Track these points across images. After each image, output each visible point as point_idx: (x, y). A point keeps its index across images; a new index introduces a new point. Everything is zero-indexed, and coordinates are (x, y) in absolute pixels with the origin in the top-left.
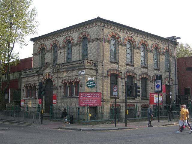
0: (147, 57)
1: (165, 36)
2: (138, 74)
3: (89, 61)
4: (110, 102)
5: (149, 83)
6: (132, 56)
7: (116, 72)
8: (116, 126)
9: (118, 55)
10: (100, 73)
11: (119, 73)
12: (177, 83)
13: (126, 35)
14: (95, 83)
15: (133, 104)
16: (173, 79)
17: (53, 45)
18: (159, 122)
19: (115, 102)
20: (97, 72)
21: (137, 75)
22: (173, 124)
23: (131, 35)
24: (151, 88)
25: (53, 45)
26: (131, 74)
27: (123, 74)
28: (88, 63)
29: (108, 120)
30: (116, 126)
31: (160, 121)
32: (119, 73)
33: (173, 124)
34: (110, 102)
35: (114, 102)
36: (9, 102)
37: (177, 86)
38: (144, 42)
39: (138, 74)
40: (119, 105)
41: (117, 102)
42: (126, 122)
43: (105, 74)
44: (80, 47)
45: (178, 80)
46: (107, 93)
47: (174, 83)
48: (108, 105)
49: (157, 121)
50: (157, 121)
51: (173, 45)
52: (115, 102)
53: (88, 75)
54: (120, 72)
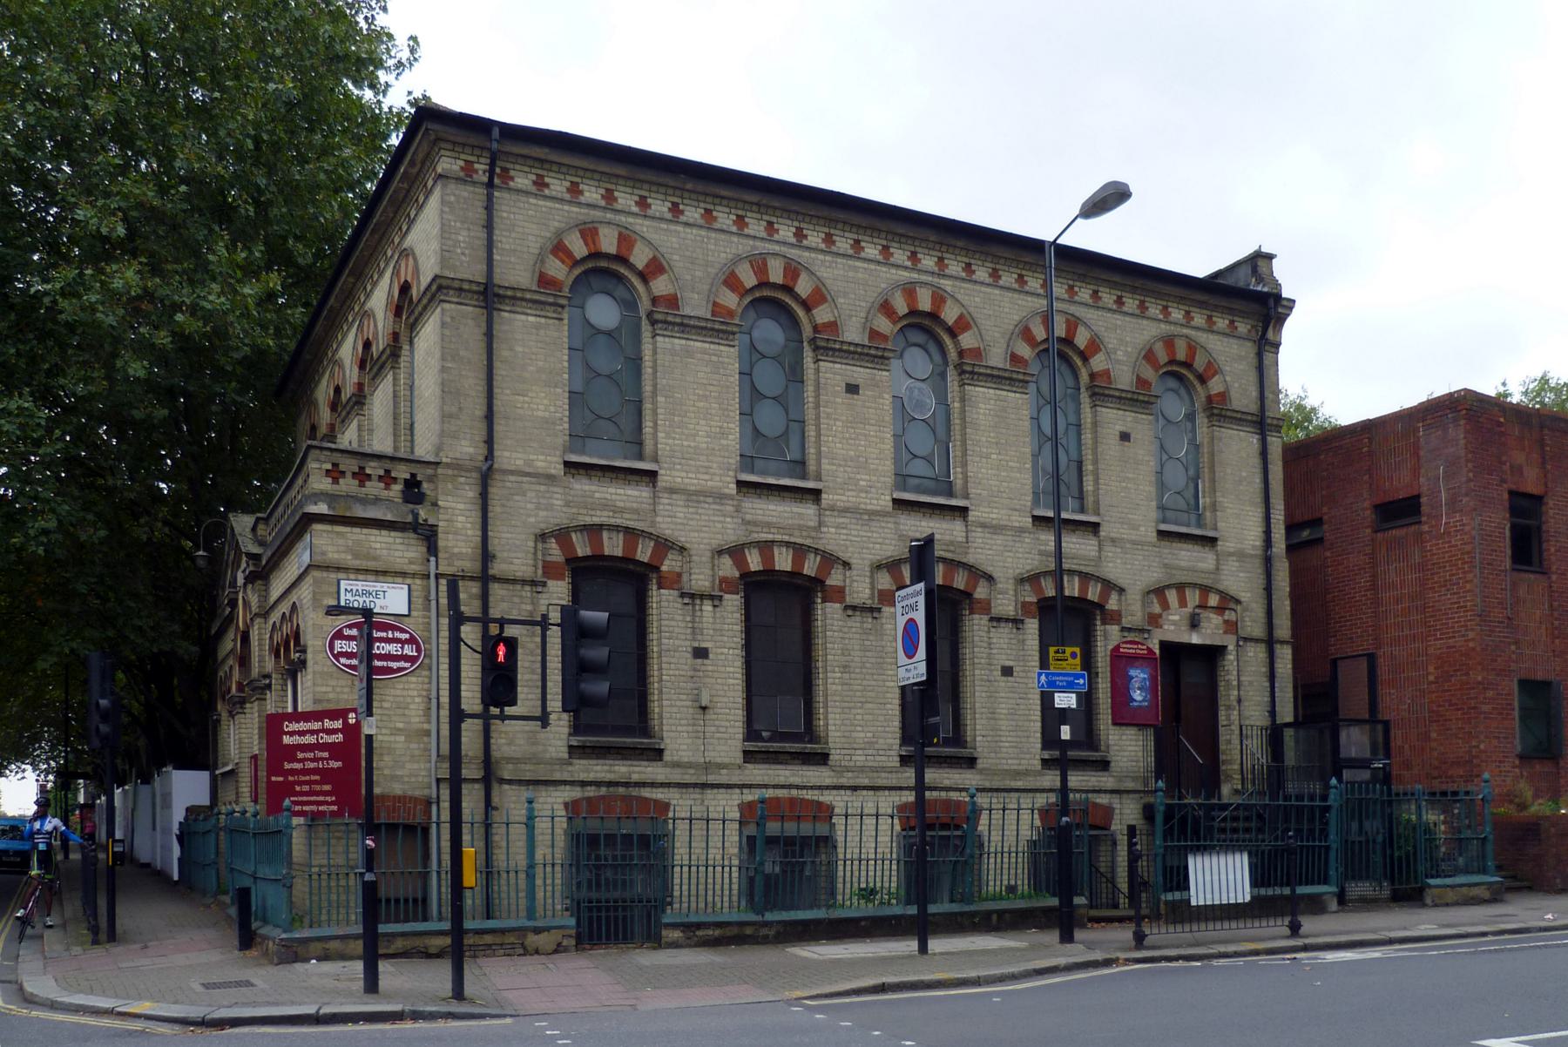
0: (963, 419)
1: (1200, 268)
2: (861, 560)
3: (350, 465)
4: (565, 783)
5: (976, 628)
7: (1084, 589)
8: (372, 984)
9: (655, 412)
10: (460, 556)
11: (1105, 594)
12: (1283, 628)
13: (741, 246)
14: (412, 641)
16: (1245, 596)
18: (923, 949)
19: (1064, 790)
20: (429, 537)
22: (248, 984)
24: (1007, 671)
28: (335, 474)
29: (703, 919)
30: (372, 984)
31: (936, 945)
32: (1105, 594)
33: (248, 984)
34: (565, 783)
37: (1285, 655)
38: (925, 304)
39: (861, 560)
40: (664, 807)
45: (1296, 596)
47: (1253, 624)
48: (553, 802)
49: (913, 945)
50: (913, 945)
51: (1243, 327)
52: (1064, 790)
53: (338, 569)
54: (1109, 586)
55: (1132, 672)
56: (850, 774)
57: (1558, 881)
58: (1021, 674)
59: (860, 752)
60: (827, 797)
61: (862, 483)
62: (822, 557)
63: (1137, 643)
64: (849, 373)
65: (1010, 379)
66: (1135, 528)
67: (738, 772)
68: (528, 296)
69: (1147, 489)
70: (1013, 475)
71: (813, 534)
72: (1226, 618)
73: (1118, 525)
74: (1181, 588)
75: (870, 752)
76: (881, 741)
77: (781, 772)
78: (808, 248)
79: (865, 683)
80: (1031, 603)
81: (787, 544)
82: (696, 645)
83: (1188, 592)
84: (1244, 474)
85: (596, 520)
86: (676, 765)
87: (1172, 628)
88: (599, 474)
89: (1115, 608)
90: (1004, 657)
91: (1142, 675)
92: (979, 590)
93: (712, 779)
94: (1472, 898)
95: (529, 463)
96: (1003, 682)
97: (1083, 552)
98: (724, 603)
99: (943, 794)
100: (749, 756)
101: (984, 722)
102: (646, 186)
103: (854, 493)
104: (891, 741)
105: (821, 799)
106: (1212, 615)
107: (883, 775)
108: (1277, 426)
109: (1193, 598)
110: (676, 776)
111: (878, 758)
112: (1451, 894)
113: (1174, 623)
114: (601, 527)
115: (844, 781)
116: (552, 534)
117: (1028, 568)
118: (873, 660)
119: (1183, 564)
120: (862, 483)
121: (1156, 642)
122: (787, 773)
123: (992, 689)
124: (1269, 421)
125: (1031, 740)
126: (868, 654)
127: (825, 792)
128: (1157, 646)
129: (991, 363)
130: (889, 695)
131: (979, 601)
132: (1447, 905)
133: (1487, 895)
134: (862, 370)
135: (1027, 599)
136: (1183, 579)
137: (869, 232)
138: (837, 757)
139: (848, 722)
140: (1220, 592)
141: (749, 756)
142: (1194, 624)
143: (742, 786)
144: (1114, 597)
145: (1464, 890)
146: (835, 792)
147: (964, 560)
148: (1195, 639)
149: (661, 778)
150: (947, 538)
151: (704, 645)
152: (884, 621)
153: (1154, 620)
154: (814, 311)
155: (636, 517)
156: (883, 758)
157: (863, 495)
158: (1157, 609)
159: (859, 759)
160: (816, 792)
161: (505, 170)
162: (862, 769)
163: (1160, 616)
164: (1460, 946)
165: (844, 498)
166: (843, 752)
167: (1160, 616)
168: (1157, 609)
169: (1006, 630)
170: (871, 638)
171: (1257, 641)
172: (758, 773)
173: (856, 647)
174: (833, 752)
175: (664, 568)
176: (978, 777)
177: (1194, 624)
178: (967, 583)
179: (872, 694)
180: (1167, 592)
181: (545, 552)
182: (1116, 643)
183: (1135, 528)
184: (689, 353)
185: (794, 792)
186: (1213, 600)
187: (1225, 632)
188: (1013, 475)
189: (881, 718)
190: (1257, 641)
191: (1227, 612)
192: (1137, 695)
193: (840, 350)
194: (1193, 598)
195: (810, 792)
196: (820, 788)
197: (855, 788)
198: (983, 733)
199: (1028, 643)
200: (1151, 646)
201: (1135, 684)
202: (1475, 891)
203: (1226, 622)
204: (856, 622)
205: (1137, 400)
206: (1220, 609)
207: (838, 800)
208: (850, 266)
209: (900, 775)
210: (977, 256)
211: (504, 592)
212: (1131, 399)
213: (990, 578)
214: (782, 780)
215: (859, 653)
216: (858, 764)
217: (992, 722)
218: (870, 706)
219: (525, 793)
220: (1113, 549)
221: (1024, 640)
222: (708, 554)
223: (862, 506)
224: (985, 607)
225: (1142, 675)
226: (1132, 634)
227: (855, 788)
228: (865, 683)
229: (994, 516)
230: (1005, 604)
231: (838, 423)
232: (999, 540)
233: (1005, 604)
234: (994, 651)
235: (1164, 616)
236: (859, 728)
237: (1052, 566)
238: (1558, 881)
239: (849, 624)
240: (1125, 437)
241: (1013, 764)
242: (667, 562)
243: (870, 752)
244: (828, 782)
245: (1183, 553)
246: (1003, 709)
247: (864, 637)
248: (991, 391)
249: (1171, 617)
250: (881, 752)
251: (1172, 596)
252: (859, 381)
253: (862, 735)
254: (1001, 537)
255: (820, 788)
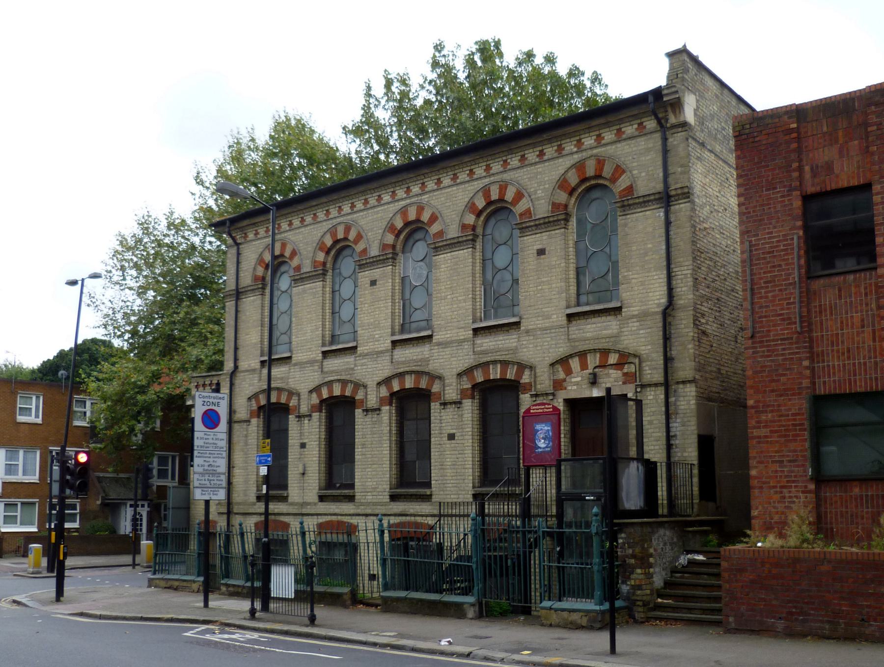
2: (371, 383)
6: (641, 200)
15: (346, 519)
17: (400, 232)
19: (267, 513)
21: (365, 387)
23: (339, 220)
24: (451, 437)
25: (400, 232)
26: (337, 391)
27: (304, 396)
32: (289, 398)
35: (261, 514)
36: (615, 521)
39: (371, 383)
41: (272, 514)
42: (57, 569)
43: (242, 412)
44: (263, 300)
46: (246, 482)
52: (267, 513)
55: (538, 427)
56: (362, 507)
57: (731, 619)
58: (460, 438)
59: (369, 494)
60: (354, 521)
61: (377, 336)
62: (518, 365)
63: (544, 404)
64: (372, 275)
65: (459, 242)
66: (548, 317)
67: (314, 507)
68: (249, 288)
69: (558, 285)
70: (460, 305)
71: (351, 372)
72: (625, 371)
73: (534, 319)
74: (582, 355)
75: (375, 493)
76: (380, 486)
77: (332, 507)
78: (284, 232)
79: (373, 453)
80: (467, 389)
81: (339, 380)
82: (301, 441)
83: (590, 358)
84: (650, 246)
85: (401, 370)
86: (292, 504)
87: (575, 387)
88: (417, 342)
89: (527, 381)
90: (450, 428)
91: (546, 428)
92: (434, 386)
93: (304, 511)
94: (571, 623)
95: (249, 365)
96: (449, 444)
97: (506, 345)
98: (313, 418)
99: (413, 518)
100: (322, 498)
101: (436, 471)
102: (289, 216)
103: (371, 344)
104: (385, 486)
105: (352, 521)
106: (611, 371)
107: (379, 507)
108: (684, 194)
109: (593, 360)
110: (292, 510)
111: (379, 497)
112: (554, 616)
113: (577, 384)
114: (332, 381)
115: (359, 511)
116: (557, 362)
117: (466, 365)
118: (376, 439)
119: (588, 335)
120: (377, 336)
121: (561, 400)
122: (334, 507)
123: (442, 449)
124: (673, 193)
125: (466, 481)
126: (375, 436)
127: (354, 517)
128: (561, 404)
129: (372, 255)
130: (384, 459)
131: (435, 394)
132: (551, 625)
133: (584, 621)
134: (378, 270)
135: (465, 387)
136: (586, 347)
137: (383, 188)
138: (359, 497)
139: (364, 477)
140: (616, 351)
141: (322, 498)
142: (594, 381)
143: (317, 515)
144: (527, 373)
145: (565, 614)
146: (357, 517)
147: (426, 370)
148: (596, 393)
149: (285, 511)
150: (420, 357)
151: (305, 441)
152: (383, 415)
153: (558, 385)
154: (564, 203)
155: (408, 365)
156: (381, 497)
157: (377, 343)
158: (561, 375)
159: (369, 498)
160: (349, 517)
161: (279, 224)
162: (368, 504)
163: (564, 380)
164: (319, 649)
165: (367, 348)
166: (362, 494)
167: (564, 380)
168: (561, 375)
169: (451, 410)
170: (376, 426)
171: (656, 385)
172: (323, 507)
173: (369, 433)
174: (357, 494)
175: (291, 405)
176: (430, 507)
177: (594, 381)
178: (428, 384)
179: (376, 459)
180: (570, 361)
181: (251, 406)
182: (528, 406)
183: (548, 317)
184: (304, 291)
185: (340, 518)
186: (613, 359)
187: (624, 383)
188: (460, 305)
189: (380, 473)
190: (656, 385)
191: (626, 366)
192: (542, 444)
193: (367, 263)
194: (593, 360)
195: (346, 517)
196: (350, 515)
197: (367, 515)
198: (436, 478)
199: (465, 416)
200: (556, 404)
201: (540, 435)
202: (575, 617)
203: (625, 374)
204: (451, 409)
205: (549, 222)
206: (619, 365)
207: (360, 522)
208: (374, 212)
209: (387, 507)
210: (441, 172)
211: (238, 427)
212: (544, 223)
213: (440, 378)
214: (332, 511)
215: (370, 436)
216: (369, 501)
217: (442, 471)
218: (375, 466)
219: (299, 519)
220: (527, 338)
221: (462, 415)
222: (307, 393)
223: (376, 350)
224: (439, 396)
225: (546, 428)
226: (541, 398)
227: (367, 515)
228: (373, 453)
229: (448, 336)
230: (372, 401)
231: (366, 305)
232: (448, 351)
233: (451, 394)
234: (444, 425)
235: (568, 380)
236: (369, 480)
237: (266, 387)
238: (731, 619)
239: (366, 420)
240: (541, 252)
241: (453, 498)
242: (292, 401)
243: (375, 493)
244: (352, 512)
245: (589, 326)
246: (448, 462)
247: (373, 426)
248: (449, 254)
249: (574, 380)
250: (380, 494)
251: (575, 363)
252: (377, 277)
253: (371, 483)
254: (449, 349)
255: (350, 515)
